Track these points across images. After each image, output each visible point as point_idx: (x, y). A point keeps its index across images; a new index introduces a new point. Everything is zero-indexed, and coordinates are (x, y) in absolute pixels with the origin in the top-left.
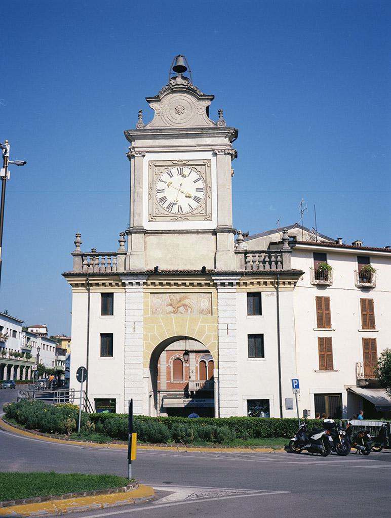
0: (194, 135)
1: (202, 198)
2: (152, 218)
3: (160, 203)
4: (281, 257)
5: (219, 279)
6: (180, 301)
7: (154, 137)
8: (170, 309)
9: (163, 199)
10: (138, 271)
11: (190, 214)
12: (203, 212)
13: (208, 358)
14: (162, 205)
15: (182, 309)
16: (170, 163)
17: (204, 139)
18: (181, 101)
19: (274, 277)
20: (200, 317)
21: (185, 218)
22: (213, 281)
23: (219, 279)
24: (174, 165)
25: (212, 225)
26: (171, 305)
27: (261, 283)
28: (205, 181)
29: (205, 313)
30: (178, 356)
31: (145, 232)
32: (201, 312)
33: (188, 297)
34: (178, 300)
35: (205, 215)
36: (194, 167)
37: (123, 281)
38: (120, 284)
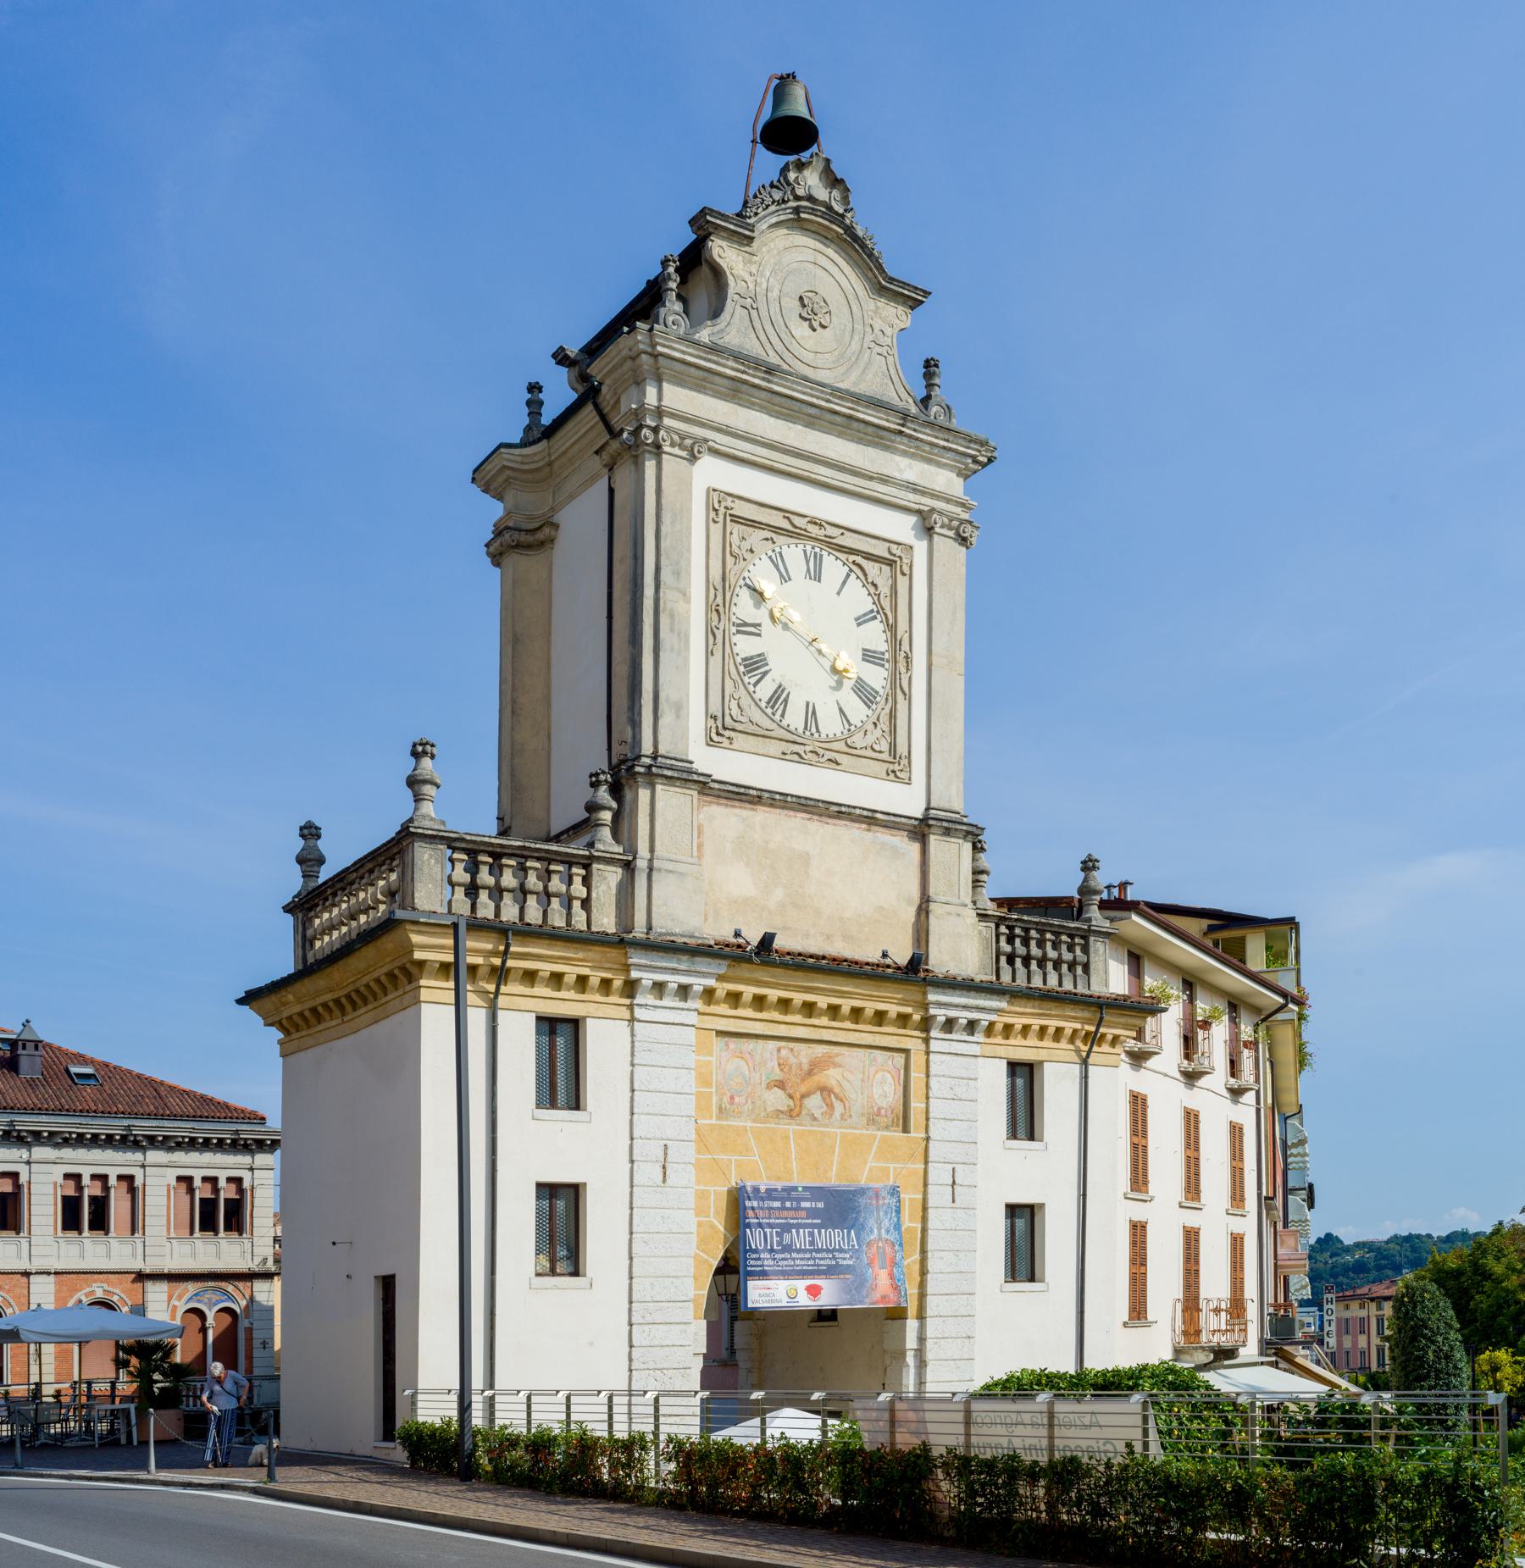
0: (870, 429)
1: (881, 691)
2: (721, 730)
3: (746, 679)
4: (586, 881)
5: (965, 1007)
6: (810, 1073)
7: (736, 391)
8: (777, 1099)
9: (755, 665)
10: (680, 940)
11: (841, 746)
12: (885, 746)
13: (215, 1298)
14: (751, 688)
15: (814, 1103)
16: (778, 520)
17: (897, 458)
18: (820, 272)
19: (1086, 1014)
20: (876, 1136)
21: (827, 755)
22: (628, 971)
23: (965, 1007)
24: (796, 534)
25: (908, 801)
26: (781, 1085)
27: (567, 979)
28: (892, 628)
29: (883, 1120)
30: (99, 1294)
31: (705, 786)
32: (873, 1119)
33: (837, 1060)
34: (806, 1067)
35: (885, 756)
36: (859, 559)
37: (634, 974)
38: (618, 983)
